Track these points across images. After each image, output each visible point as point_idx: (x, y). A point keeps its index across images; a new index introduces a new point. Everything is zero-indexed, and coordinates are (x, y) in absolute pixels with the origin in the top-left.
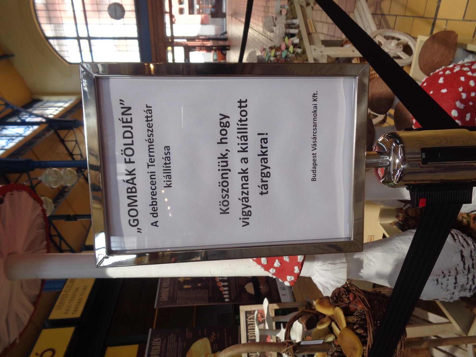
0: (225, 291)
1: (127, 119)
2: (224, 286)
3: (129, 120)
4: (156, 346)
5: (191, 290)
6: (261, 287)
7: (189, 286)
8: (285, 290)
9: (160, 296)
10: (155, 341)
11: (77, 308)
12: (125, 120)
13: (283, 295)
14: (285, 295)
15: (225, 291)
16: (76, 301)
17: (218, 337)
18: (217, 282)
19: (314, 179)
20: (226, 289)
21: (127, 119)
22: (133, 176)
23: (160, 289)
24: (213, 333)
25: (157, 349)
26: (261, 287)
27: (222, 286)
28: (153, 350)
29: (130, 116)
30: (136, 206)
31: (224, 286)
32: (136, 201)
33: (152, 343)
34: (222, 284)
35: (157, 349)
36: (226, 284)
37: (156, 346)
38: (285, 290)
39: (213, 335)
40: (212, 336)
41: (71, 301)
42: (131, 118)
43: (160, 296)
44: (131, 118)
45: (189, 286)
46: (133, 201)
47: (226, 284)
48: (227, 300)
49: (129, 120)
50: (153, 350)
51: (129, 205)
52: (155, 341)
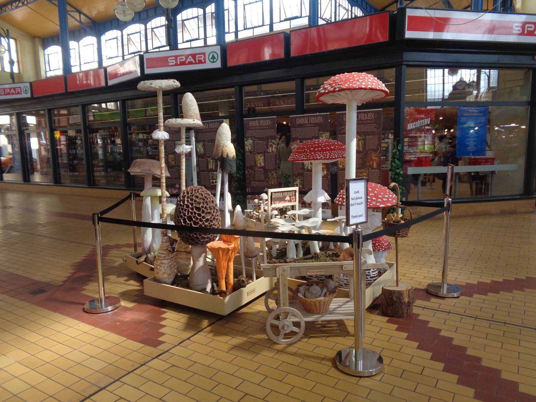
25: (365, 117)
28: (365, 115)
35: (365, 117)
50: (365, 115)
52: (371, 115)
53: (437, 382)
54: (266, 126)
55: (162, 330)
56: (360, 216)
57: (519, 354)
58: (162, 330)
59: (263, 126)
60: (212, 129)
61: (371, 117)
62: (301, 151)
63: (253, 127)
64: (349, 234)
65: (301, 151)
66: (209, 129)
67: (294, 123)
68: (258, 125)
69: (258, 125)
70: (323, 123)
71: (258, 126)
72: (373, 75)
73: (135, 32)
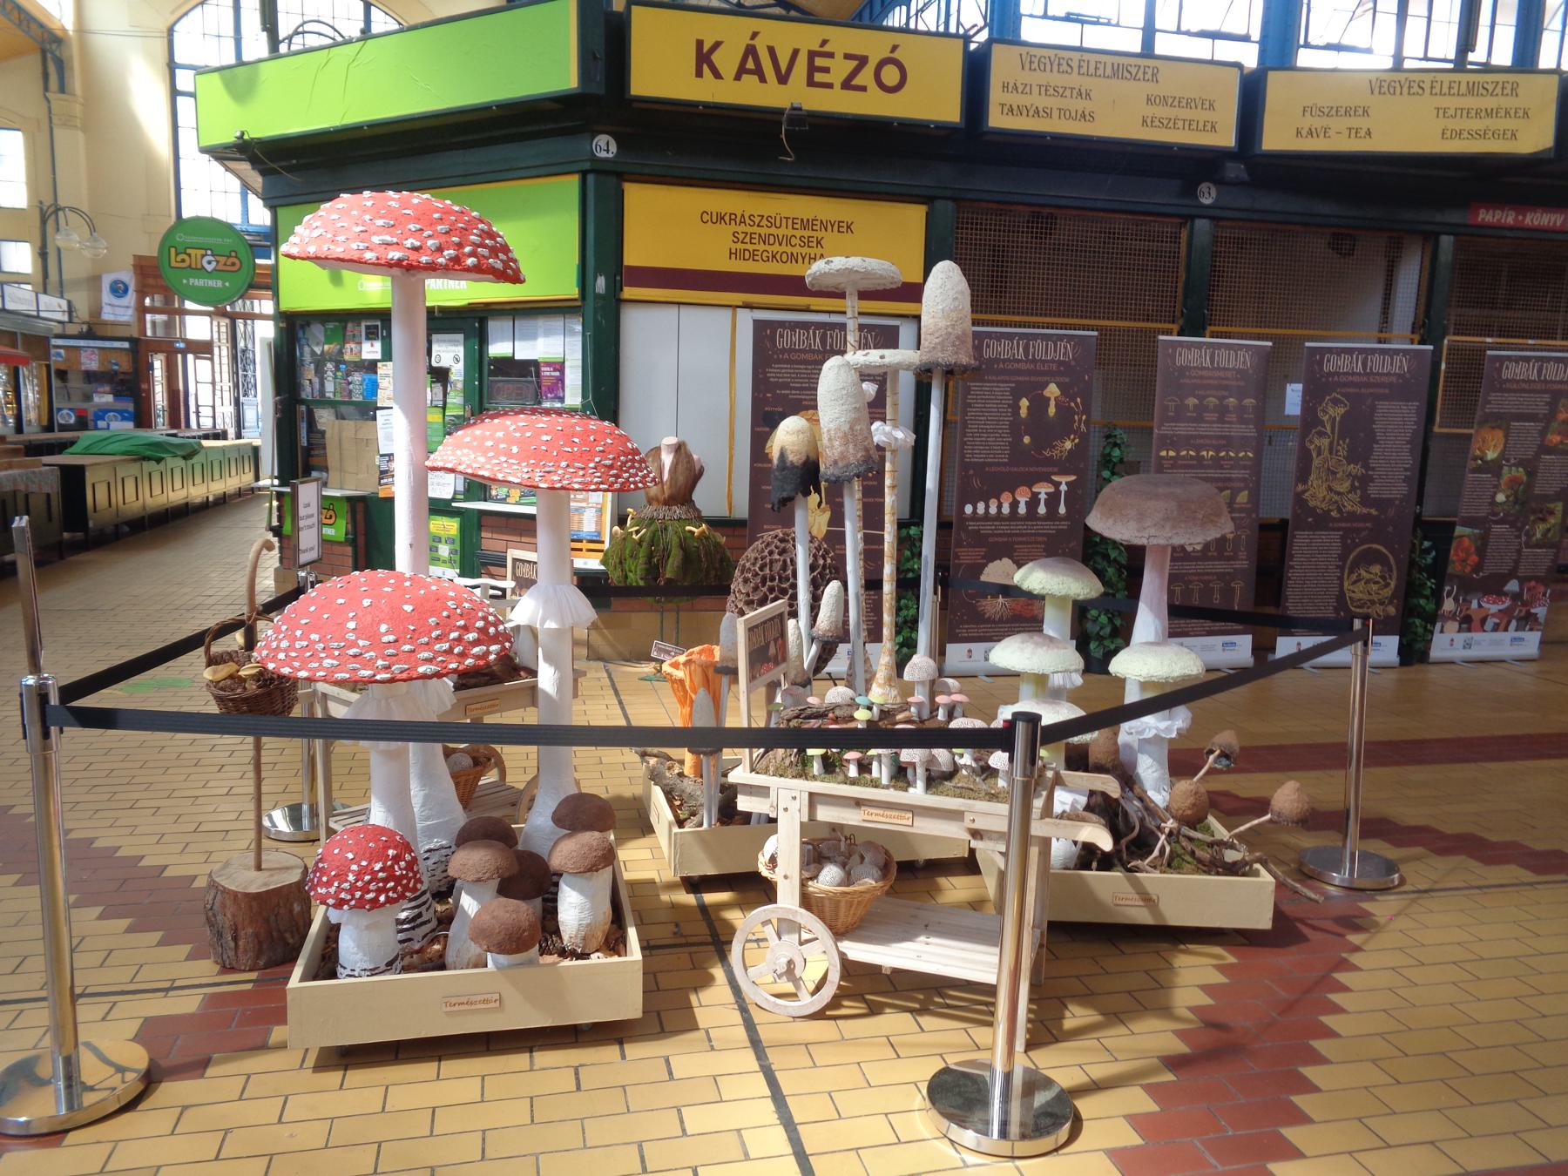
0: (1000, 506)
2: (1014, 505)
3: (811, 244)
4: (1055, 351)
6: (1001, 600)
7: (1023, 413)
8: (1464, 647)
9: (999, 337)
10: (1066, 348)
11: (1021, 111)
13: (1452, 640)
14: (1452, 645)
15: (1000, 506)
16: (1041, 102)
19: (307, 1050)
20: (1006, 510)
23: (1361, 351)
25: (1046, 353)
26: (1001, 600)
27: (1014, 498)
28: (1047, 345)
31: (1014, 505)
33: (1241, 350)
34: (1023, 501)
35: (1046, 353)
36: (1022, 510)
37: (1055, 351)
38: (1464, 647)
41: (1045, 89)
43: (999, 337)
45: (1023, 413)
46: (783, 71)
47: (1022, 510)
48: (969, 509)
49: (811, 244)
50: (1047, 345)
52: (1066, 348)
53: (532, 1117)
54: (1388, 374)
55: (1309, 1072)
56: (312, 549)
57: (741, 1136)
58: (1309, 1072)
59: (1378, 374)
60: (1555, 382)
61: (1400, 367)
62: (1184, 453)
63: (1338, 374)
64: (1005, 721)
65: (1184, 453)
66: (1214, 369)
67: (1316, 367)
68: (1208, 364)
69: (1208, 364)
70: (1073, 363)
71: (1359, 374)
72: (306, 218)
73: (1442, 57)
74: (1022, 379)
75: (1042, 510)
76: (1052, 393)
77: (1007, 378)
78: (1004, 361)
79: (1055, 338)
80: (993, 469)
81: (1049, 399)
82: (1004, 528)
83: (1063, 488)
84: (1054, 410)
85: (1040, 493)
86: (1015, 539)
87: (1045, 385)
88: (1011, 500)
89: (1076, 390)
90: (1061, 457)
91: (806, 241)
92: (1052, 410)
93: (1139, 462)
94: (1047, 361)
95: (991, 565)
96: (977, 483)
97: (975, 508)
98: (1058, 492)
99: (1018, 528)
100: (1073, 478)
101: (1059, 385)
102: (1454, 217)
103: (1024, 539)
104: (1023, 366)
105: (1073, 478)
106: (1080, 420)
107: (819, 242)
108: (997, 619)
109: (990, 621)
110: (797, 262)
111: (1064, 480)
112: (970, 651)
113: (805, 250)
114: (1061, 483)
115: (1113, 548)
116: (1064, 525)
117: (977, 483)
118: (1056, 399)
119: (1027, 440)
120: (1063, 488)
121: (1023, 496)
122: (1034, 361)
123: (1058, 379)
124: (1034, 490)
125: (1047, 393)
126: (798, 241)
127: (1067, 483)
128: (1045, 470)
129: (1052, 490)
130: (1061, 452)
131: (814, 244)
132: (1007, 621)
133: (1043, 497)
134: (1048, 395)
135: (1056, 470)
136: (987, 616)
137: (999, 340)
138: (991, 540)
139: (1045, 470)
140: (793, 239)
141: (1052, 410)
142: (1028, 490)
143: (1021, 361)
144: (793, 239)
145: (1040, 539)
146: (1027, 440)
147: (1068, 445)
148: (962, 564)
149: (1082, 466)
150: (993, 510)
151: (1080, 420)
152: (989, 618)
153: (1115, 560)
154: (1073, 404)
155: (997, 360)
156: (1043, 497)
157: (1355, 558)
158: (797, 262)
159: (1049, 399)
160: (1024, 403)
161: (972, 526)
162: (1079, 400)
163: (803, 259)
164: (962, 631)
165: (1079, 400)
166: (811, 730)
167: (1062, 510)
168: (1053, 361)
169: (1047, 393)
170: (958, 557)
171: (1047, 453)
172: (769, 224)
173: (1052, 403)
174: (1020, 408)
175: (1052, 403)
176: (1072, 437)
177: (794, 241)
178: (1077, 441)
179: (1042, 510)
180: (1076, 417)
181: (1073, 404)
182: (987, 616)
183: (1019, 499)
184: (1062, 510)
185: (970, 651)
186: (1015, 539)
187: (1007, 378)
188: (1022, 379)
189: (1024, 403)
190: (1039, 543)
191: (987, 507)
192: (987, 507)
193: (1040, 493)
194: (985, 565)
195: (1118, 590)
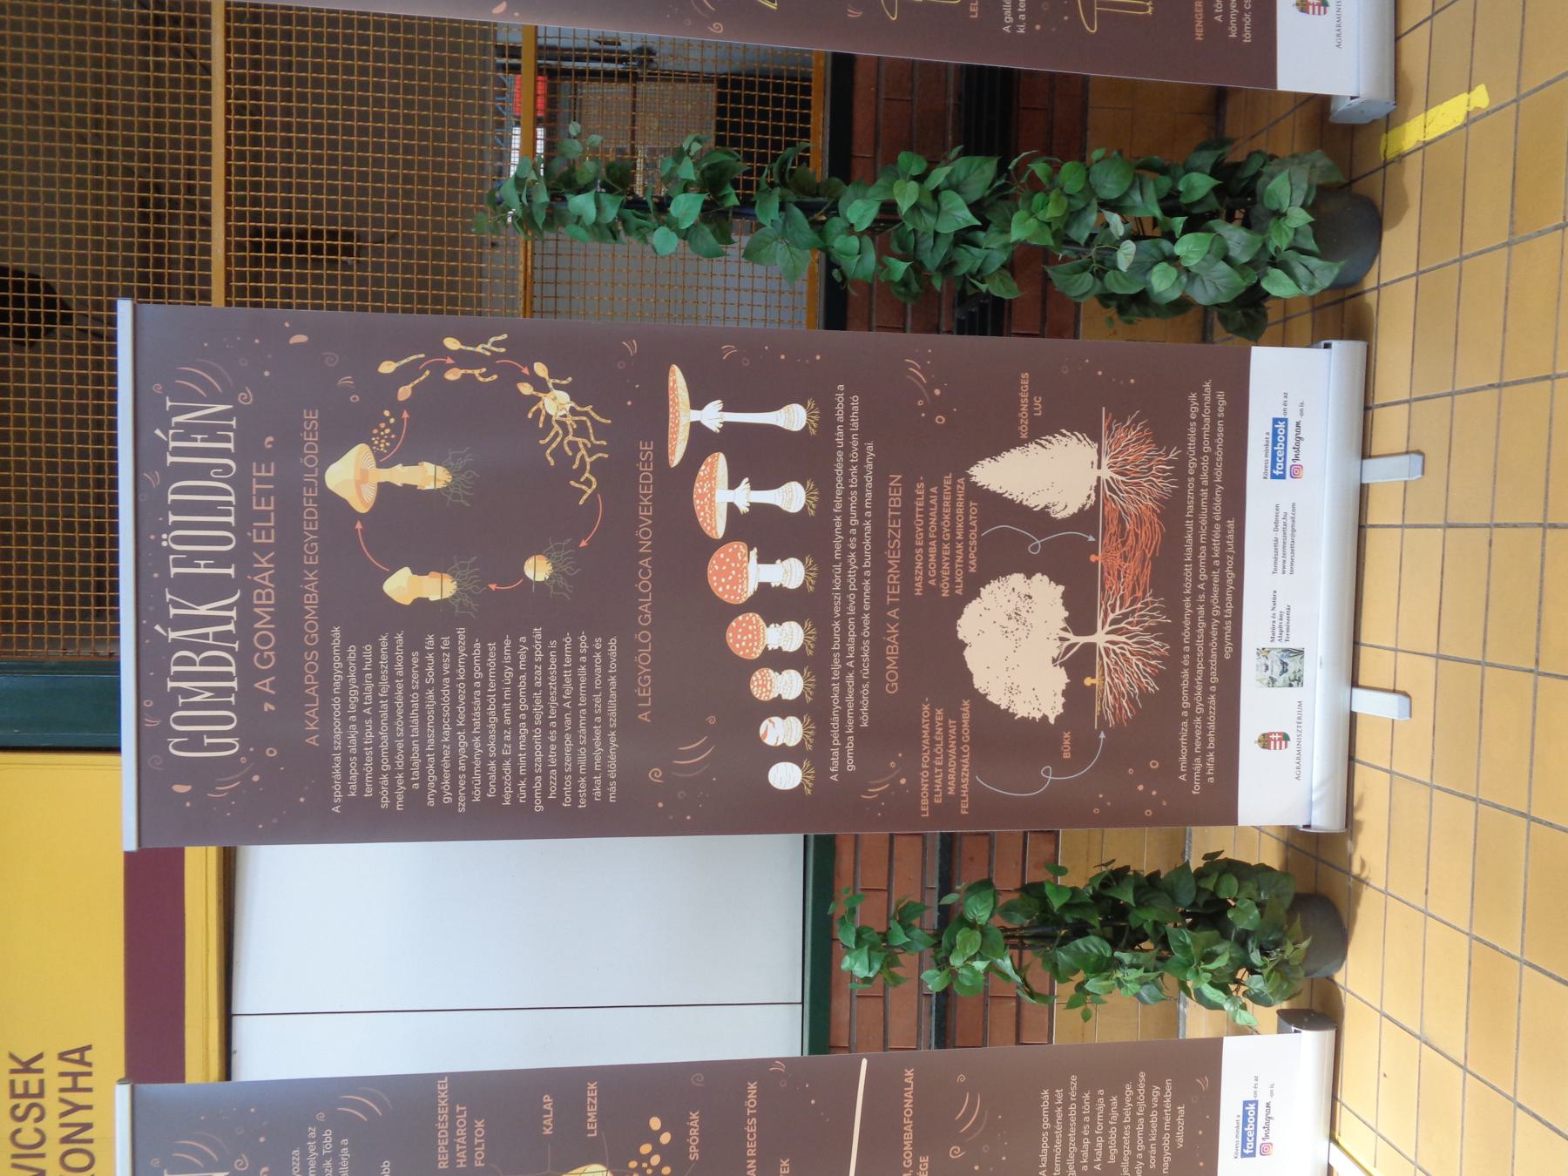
1: (26, 1084)
2: (772, 604)
3: (34, 1089)
4: (202, 472)
5: (461, 633)
7: (438, 587)
10: (188, 431)
12: (19, 1090)
15: (777, 660)
17: (694, 1154)
18: (714, 545)
20: (789, 636)
21: (26, 1084)
22: (67, 1096)
24: (655, 1123)
27: (752, 605)
28: (180, 508)
29: (40, 1076)
30: (90, 1141)
31: (772, 604)
32: (87, 1126)
36: (790, 573)
37: (202, 472)
39: (653, 1137)
40: (646, 1149)
42: (41, 1083)
44: (41, 1083)
45: (438, 587)
47: (790, 573)
48: (785, 776)
49: (34, 1089)
50: (180, 508)
51: (65, 1140)
52: (188, 431)
70: (246, 397)
74: (311, 602)
75: (791, 497)
76: (363, 478)
77: (311, 658)
78: (248, 673)
79: (152, 478)
80: (644, 691)
81: (385, 489)
82: (852, 640)
83: (713, 416)
84: (429, 467)
85: (732, 508)
86: (893, 592)
87: (334, 505)
88: (755, 618)
89: (347, 380)
90: (600, 430)
91: (25, 1103)
92: (428, 476)
93: (496, 46)
94: (243, 507)
95: (979, 683)
96: (695, 754)
97: (783, 753)
98: (733, 441)
99: (851, 576)
100: (677, 379)
101: (333, 451)
102: (1198, 911)
103: (894, 559)
104: (265, 604)
105: (677, 379)
106: (462, 359)
107: (26, 1067)
108: (1164, 648)
109: (1168, 676)
110: (87, 1126)
111: (684, 416)
112: (1265, 741)
113: (52, 1104)
114: (696, 428)
115: (937, 213)
116: (848, 407)
117: (695, 754)
118: (383, 462)
119: (538, 569)
120: (713, 416)
121: (742, 572)
122: (243, 556)
123: (311, 454)
124: (719, 530)
125: (361, 500)
126: (28, 1125)
127: (697, 403)
128: (646, 492)
129: (719, 465)
130: (581, 430)
131: (33, 1079)
132: (1174, 610)
133: (744, 497)
134: (370, 495)
135: (647, 449)
136: (1152, 686)
137: (169, 702)
138: (893, 686)
139: (646, 492)
140: (20, 1138)
141: (428, 476)
142: (720, 554)
143: (245, 607)
144: (20, 1138)
145: (895, 499)
146: (538, 569)
147: (557, 403)
148: (973, 783)
149: (632, 347)
150: (790, 685)
151: (462, 359)
152: (1158, 677)
153: (976, 207)
154: (404, 392)
155: (248, 700)
156: (744, 497)
157: (202, 1150)
158: (87, 1126)
159: (385, 489)
160: (402, 586)
161: (844, 759)
162: (387, 367)
163: (76, 1108)
164: (1198, 772)
165: (387, 367)
166: (860, 422)
167: (793, 417)
168: (240, 483)
169: (361, 500)
170: (952, 802)
171: (588, 486)
172: (35, 1113)
173: (401, 475)
174: (421, 603)
175: (401, 475)
176: (526, 389)
177: (28, 1136)
178: (541, 369)
179: (791, 497)
180: (453, 375)
181: (404, 392)
182: (1152, 686)
183: (751, 588)
184: (793, 417)
185: (1265, 741)
186: (893, 592)
187: (311, 658)
188: (311, 602)
189: (402, 586)
190: (909, 497)
191: (781, 708)
192: (781, 708)
193: (732, 508)
194: (980, 700)
195: (1089, 189)
